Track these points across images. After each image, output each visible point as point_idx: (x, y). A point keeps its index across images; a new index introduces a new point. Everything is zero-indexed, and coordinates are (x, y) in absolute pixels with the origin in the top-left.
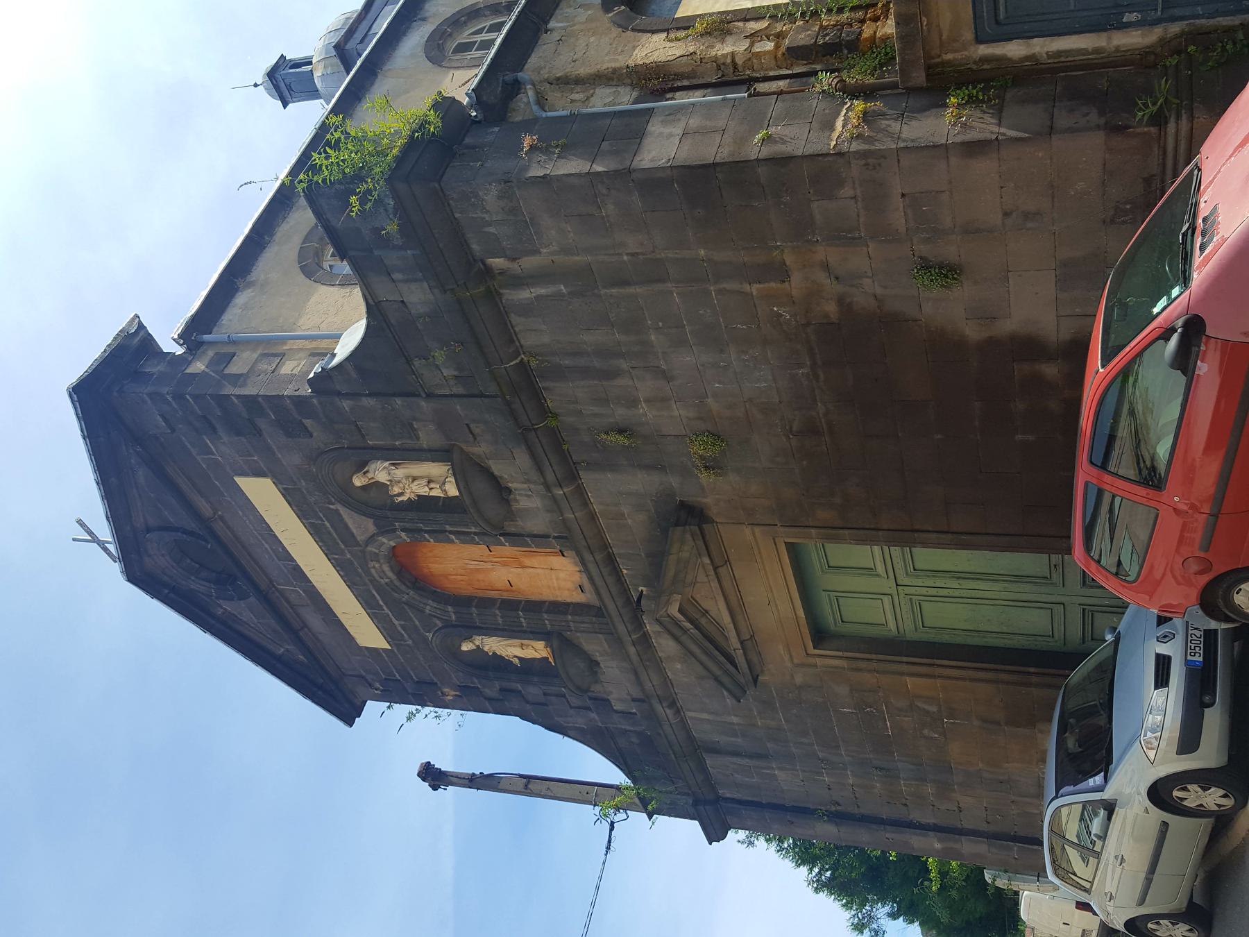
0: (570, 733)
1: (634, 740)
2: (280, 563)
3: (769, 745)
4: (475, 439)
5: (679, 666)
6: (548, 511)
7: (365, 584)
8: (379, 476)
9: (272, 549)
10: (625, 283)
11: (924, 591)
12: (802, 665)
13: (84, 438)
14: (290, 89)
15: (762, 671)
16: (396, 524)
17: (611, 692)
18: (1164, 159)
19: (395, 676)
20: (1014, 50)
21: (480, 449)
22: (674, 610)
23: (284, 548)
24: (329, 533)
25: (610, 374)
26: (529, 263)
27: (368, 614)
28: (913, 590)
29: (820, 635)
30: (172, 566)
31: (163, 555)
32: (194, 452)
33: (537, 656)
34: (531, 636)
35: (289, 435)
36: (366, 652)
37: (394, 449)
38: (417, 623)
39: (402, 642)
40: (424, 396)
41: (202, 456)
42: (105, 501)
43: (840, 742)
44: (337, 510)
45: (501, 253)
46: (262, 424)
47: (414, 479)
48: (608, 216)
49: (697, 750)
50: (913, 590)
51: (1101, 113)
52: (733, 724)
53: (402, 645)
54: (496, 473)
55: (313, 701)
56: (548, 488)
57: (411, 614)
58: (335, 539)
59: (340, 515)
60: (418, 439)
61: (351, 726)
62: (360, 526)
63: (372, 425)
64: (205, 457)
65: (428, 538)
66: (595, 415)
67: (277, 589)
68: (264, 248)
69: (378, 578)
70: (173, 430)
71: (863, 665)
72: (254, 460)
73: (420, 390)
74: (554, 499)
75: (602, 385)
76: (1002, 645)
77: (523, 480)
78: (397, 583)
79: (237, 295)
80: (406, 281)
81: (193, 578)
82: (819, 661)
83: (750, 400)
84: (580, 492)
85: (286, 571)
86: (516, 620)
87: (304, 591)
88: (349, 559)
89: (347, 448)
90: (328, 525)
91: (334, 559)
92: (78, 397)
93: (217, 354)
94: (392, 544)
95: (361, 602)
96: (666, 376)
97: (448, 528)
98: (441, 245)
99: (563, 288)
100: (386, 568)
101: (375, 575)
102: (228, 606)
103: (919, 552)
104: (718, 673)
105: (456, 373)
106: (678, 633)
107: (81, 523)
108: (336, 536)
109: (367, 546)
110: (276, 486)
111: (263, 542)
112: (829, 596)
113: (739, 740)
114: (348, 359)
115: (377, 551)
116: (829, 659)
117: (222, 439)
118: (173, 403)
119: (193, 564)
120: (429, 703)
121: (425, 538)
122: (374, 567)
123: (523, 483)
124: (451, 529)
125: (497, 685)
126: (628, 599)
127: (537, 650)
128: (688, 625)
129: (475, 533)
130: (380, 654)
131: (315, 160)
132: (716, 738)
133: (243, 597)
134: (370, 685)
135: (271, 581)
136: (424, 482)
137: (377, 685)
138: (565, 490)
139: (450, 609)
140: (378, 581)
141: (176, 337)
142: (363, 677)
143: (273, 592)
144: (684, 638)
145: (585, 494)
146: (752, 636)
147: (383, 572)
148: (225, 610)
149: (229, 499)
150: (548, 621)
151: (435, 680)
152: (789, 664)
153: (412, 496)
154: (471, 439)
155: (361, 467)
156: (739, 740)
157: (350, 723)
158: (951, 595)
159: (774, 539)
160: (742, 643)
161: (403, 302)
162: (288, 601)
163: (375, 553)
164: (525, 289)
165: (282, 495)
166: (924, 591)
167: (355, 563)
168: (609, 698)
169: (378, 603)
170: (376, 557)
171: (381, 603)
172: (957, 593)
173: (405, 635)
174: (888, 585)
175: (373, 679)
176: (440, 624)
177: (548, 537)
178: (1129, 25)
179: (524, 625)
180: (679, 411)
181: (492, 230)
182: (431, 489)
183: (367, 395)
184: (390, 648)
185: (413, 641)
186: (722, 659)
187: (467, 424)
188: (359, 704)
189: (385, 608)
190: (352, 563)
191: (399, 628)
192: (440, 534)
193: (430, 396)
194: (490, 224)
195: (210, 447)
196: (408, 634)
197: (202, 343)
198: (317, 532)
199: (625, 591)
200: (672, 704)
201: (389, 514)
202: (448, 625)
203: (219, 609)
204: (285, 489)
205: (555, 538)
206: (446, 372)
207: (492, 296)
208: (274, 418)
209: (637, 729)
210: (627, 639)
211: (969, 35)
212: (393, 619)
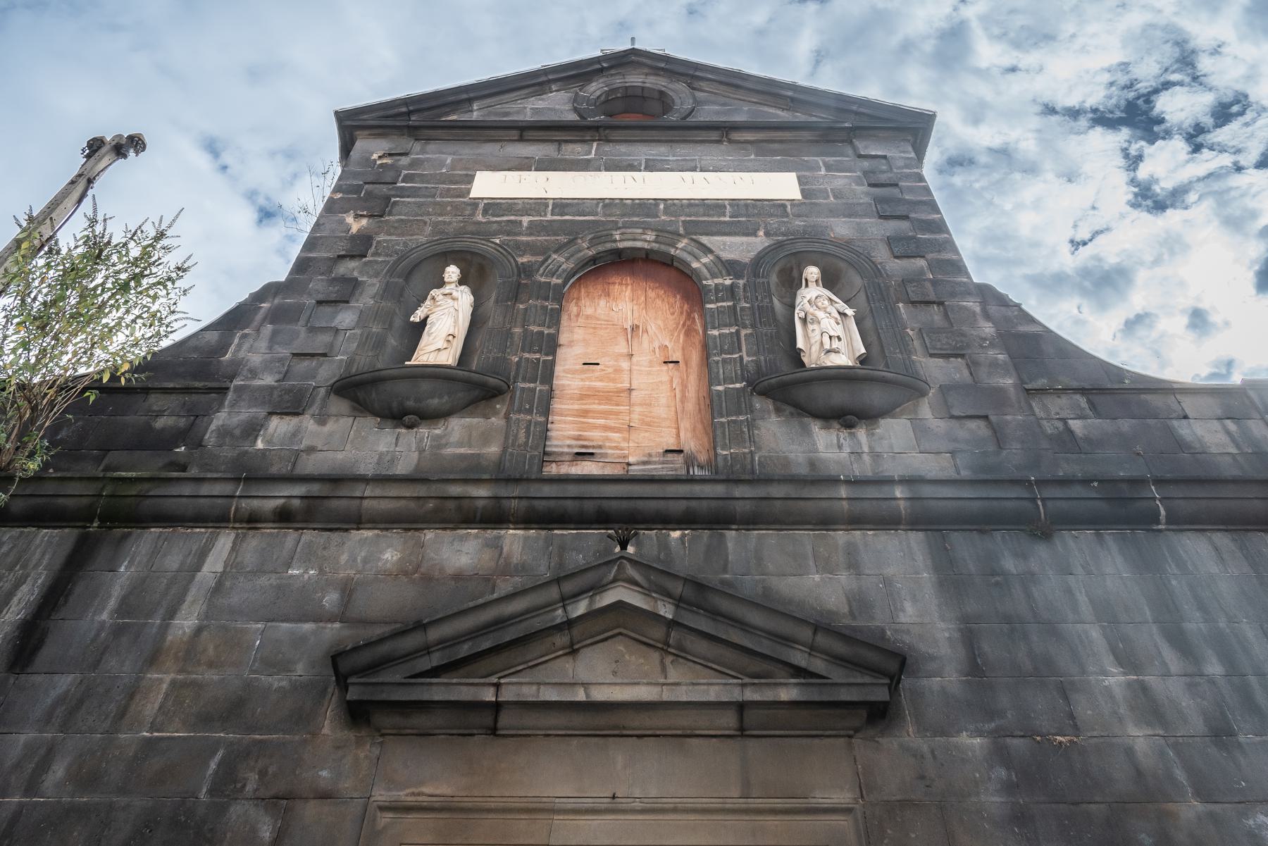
3: (65, 682)
52: (172, 613)
78: (609, 246)
104: (434, 634)
111: (675, 158)
113: (105, 616)
131: (765, 360)
144: (554, 593)
145: (872, 527)
148: (551, 92)
152: (381, 795)
156: (105, 616)
157: (336, 113)
186: (465, 650)
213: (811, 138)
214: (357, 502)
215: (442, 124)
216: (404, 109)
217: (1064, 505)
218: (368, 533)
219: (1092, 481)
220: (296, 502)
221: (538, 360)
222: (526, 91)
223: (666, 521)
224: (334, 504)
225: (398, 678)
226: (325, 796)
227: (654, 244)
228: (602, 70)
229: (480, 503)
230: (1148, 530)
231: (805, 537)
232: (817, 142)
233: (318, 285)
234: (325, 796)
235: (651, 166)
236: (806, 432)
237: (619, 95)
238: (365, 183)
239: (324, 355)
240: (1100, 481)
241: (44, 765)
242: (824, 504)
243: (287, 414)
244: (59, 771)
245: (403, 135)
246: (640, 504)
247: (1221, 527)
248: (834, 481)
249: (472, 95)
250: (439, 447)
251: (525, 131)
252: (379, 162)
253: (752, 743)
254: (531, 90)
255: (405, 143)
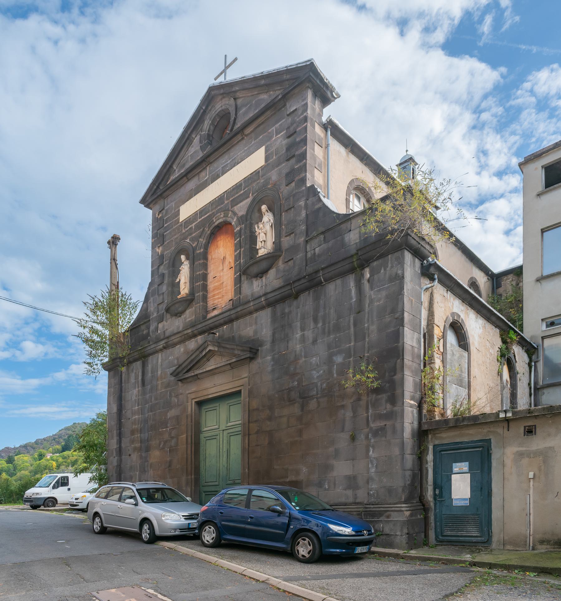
0: (145, 305)
1: (145, 332)
2: (220, 168)
4: (286, 262)
5: (182, 350)
6: (252, 295)
7: (212, 210)
8: (266, 217)
9: (228, 164)
10: (355, 325)
11: (221, 439)
12: (187, 398)
13: (286, 67)
14: (404, 168)
15: (183, 383)
16: (243, 226)
17: (167, 322)
18: (393, 504)
19: (166, 224)
20: (430, 457)
21: (280, 264)
22: (210, 348)
23: (229, 170)
24: (238, 193)
25: (316, 321)
26: (366, 286)
27: (197, 211)
28: (221, 436)
29: (200, 404)
30: (216, 111)
31: (222, 106)
32: (277, 125)
33: (181, 290)
34: (192, 287)
35: (287, 175)
36: (177, 210)
37: (281, 225)
38: (194, 235)
39: (183, 228)
40: (307, 239)
41: (275, 130)
42: (252, 77)
43: (154, 413)
44: (249, 197)
45: (372, 275)
46: (293, 161)
47: (265, 234)
48: (385, 318)
49: (144, 357)
50: (221, 436)
51: (409, 485)
53: (182, 227)
54: (269, 272)
55: (151, 184)
56: (265, 295)
57: (198, 232)
58: (234, 196)
59: (247, 198)
60: (286, 236)
61: (140, 203)
62: (242, 208)
63: (292, 215)
64: (274, 131)
65: (237, 240)
66: (297, 314)
67: (207, 166)
68: (361, 161)
69: (215, 216)
70: (288, 115)
71: (189, 419)
72: (273, 156)
73: (309, 238)
74: (260, 297)
75: (311, 317)
76: (200, 466)
77: (267, 283)
78: (213, 226)
79: (344, 147)
80: (360, 232)
81: (210, 122)
82: (189, 404)
83: (304, 375)
84: (262, 308)
85: (217, 170)
86: (199, 280)
87: (206, 180)
88: (224, 202)
89: (281, 203)
90: (242, 192)
91: (224, 195)
92: (308, 65)
93: (322, 139)
94: (233, 223)
95: (204, 207)
96: (315, 341)
97: (242, 249)
98: (378, 249)
99: (354, 300)
100: (221, 220)
101: (217, 215)
102: (196, 140)
103: (239, 438)
105: (317, 254)
106: (200, 350)
107: (236, 59)
108: (236, 196)
109: (231, 211)
110: (261, 167)
111: (231, 160)
112: (217, 406)
114: (324, 204)
115: (229, 216)
116: (191, 407)
117: (284, 140)
118: (302, 116)
119: (217, 122)
120: (153, 240)
121: (237, 239)
122: (221, 215)
123: (265, 283)
124: (242, 251)
125: (166, 272)
126: (212, 329)
127: (184, 290)
128: (204, 353)
129: (240, 262)
130: (176, 217)
132: (150, 366)
133: (202, 148)
134: (160, 212)
135: (211, 163)
136: (264, 239)
137: (160, 215)
138: (264, 302)
139: (202, 250)
140: (214, 216)
141: (331, 118)
142: (163, 209)
143: (205, 164)
144: (198, 352)
146: (199, 379)
147: (219, 219)
148: (194, 139)
149: (253, 143)
150: (199, 294)
151: (165, 243)
152: (187, 392)
153: (257, 233)
154: (286, 260)
155: (270, 209)
158: (220, 449)
159: (243, 385)
160: (197, 375)
161: (350, 231)
162: (200, 172)
163: (228, 215)
164: (354, 284)
165: (256, 170)
166: (221, 439)
167: (222, 206)
168: (164, 321)
169: (203, 216)
170: (226, 216)
171: (203, 218)
172: (221, 451)
173: (187, 229)
174: (223, 427)
175: (163, 213)
176: (194, 245)
177: (240, 294)
178: (435, 490)
179: (197, 284)
180: (298, 347)
181: (382, 271)
182: (261, 242)
183: (307, 212)
184: (180, 221)
185: (184, 233)
186: (189, 367)
187: (293, 259)
188: (150, 206)
189: (201, 219)
190: (222, 204)
191: (190, 226)
192: (238, 246)
193: (307, 242)
194: (385, 270)
195: (279, 134)
196: (188, 230)
197: (326, 131)
198: (237, 187)
199: (217, 327)
200: (165, 348)
201: (248, 222)
202: (194, 249)
203: (195, 136)
204: (259, 172)
205: (240, 297)
206: (317, 250)
207: (352, 270)
208: (296, 167)
209: (151, 334)
210: (195, 328)
211: (437, 442)
212: (195, 223)
213: (272, 114)
214: (172, 341)
215: (169, 186)
216: (155, 187)
217: (299, 287)
218: (178, 346)
219: (306, 276)
220: (164, 344)
221: (199, 284)
222: (185, 147)
223: (222, 325)
224: (170, 342)
225: (181, 375)
226: (181, 394)
227: (224, 218)
228: (205, 112)
229: (190, 334)
230: (321, 286)
231: (248, 318)
232: (275, 113)
233: (157, 280)
234: (181, 394)
235: (215, 177)
236: (252, 283)
237: (218, 120)
238: (158, 230)
239: (163, 302)
240: (308, 275)
241: (151, 398)
242: (248, 309)
243: (161, 322)
244: (153, 399)
245: (160, 199)
246: (216, 323)
247: (340, 277)
248: (249, 302)
249: (170, 164)
250: (185, 320)
251: (188, 175)
252: (159, 217)
253: (234, 369)
254: (187, 144)
255: (161, 202)
